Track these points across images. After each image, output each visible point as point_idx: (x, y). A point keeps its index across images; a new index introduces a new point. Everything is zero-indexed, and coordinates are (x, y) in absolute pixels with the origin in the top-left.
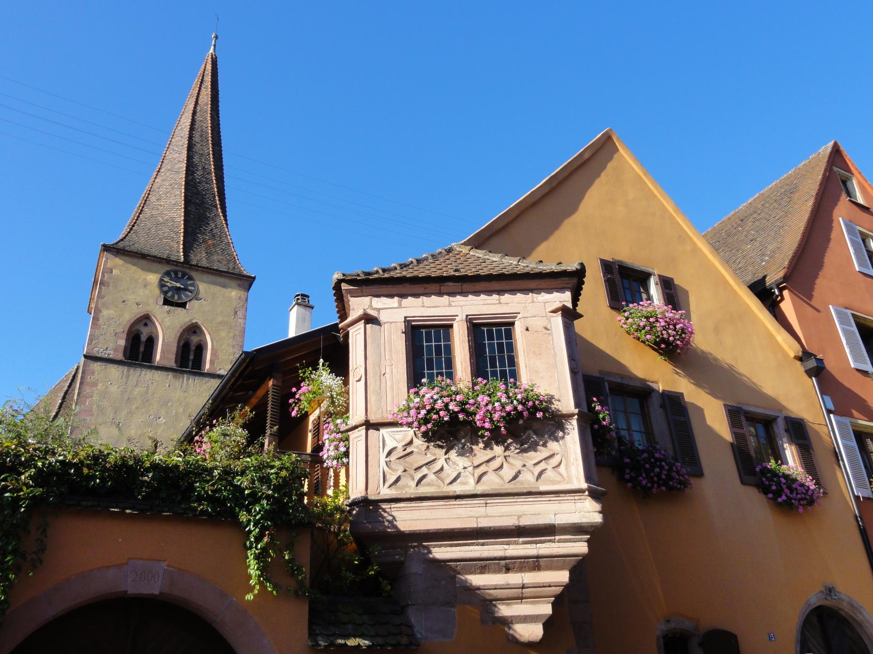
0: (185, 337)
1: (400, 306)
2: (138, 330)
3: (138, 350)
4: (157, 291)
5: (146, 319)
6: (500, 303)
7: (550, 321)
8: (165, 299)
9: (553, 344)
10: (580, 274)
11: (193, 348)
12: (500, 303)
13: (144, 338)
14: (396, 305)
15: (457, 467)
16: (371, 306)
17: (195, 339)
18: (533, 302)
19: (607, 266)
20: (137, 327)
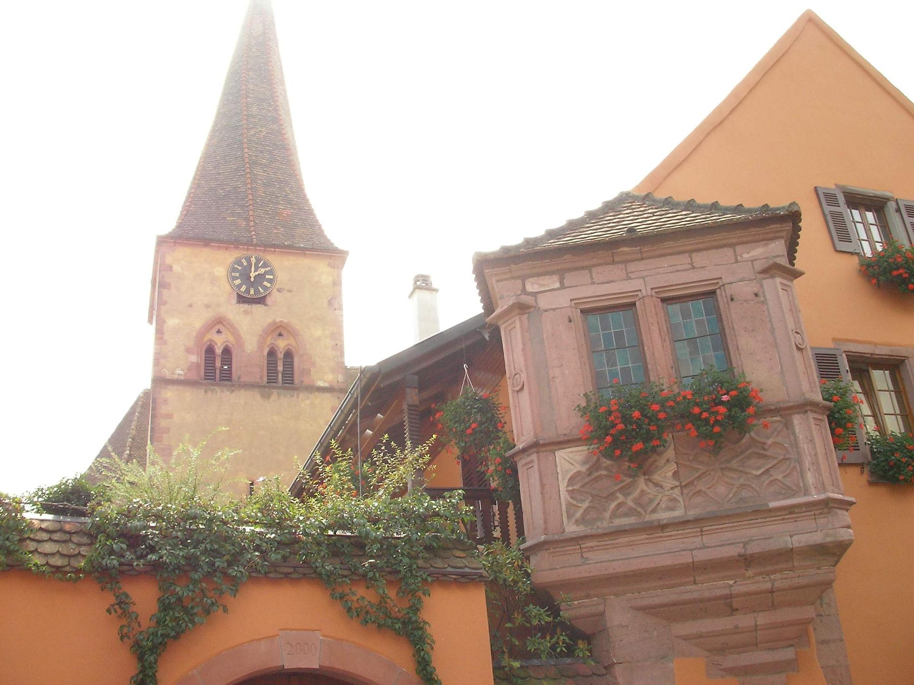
0: (269, 341)
1: (563, 287)
2: (211, 340)
3: (216, 367)
4: (228, 288)
5: (219, 323)
6: (694, 268)
7: (762, 286)
8: (239, 295)
9: (769, 315)
10: (793, 217)
11: (281, 356)
12: (694, 268)
13: (219, 351)
14: (557, 285)
15: (666, 490)
16: (524, 291)
17: (282, 345)
18: (737, 261)
19: (826, 198)
20: (208, 337)
